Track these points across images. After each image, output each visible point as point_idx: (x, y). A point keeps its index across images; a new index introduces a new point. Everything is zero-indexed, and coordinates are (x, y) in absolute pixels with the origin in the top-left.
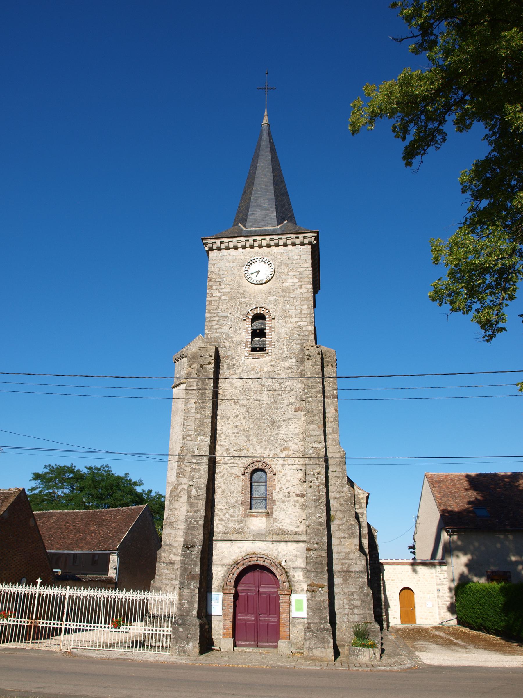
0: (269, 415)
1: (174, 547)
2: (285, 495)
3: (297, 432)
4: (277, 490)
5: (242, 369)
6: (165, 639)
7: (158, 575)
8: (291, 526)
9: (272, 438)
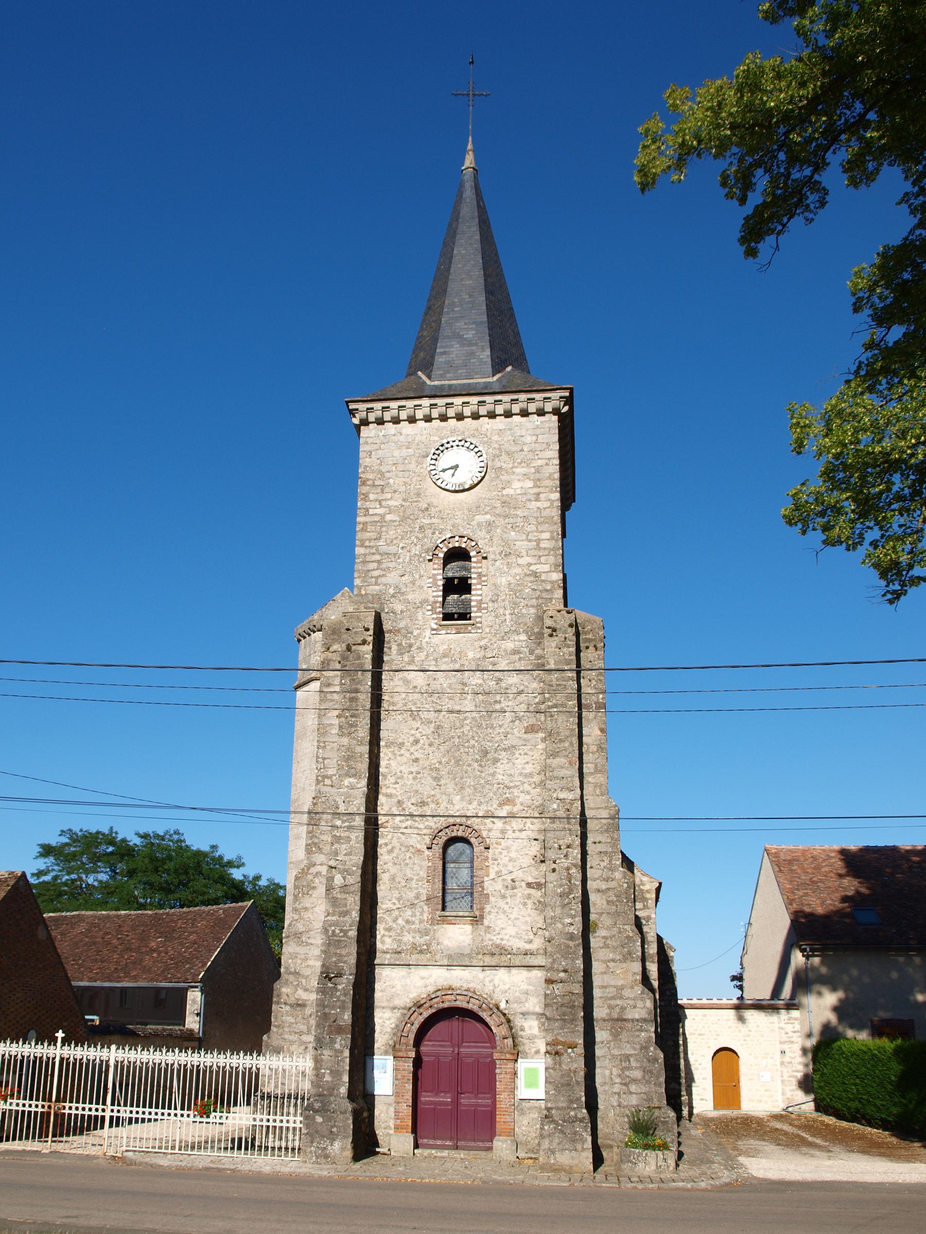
0: (476, 739)
1: (303, 976)
4: (492, 875)
6: (290, 1136)
7: (275, 1026)
8: (517, 940)
9: (482, 782)
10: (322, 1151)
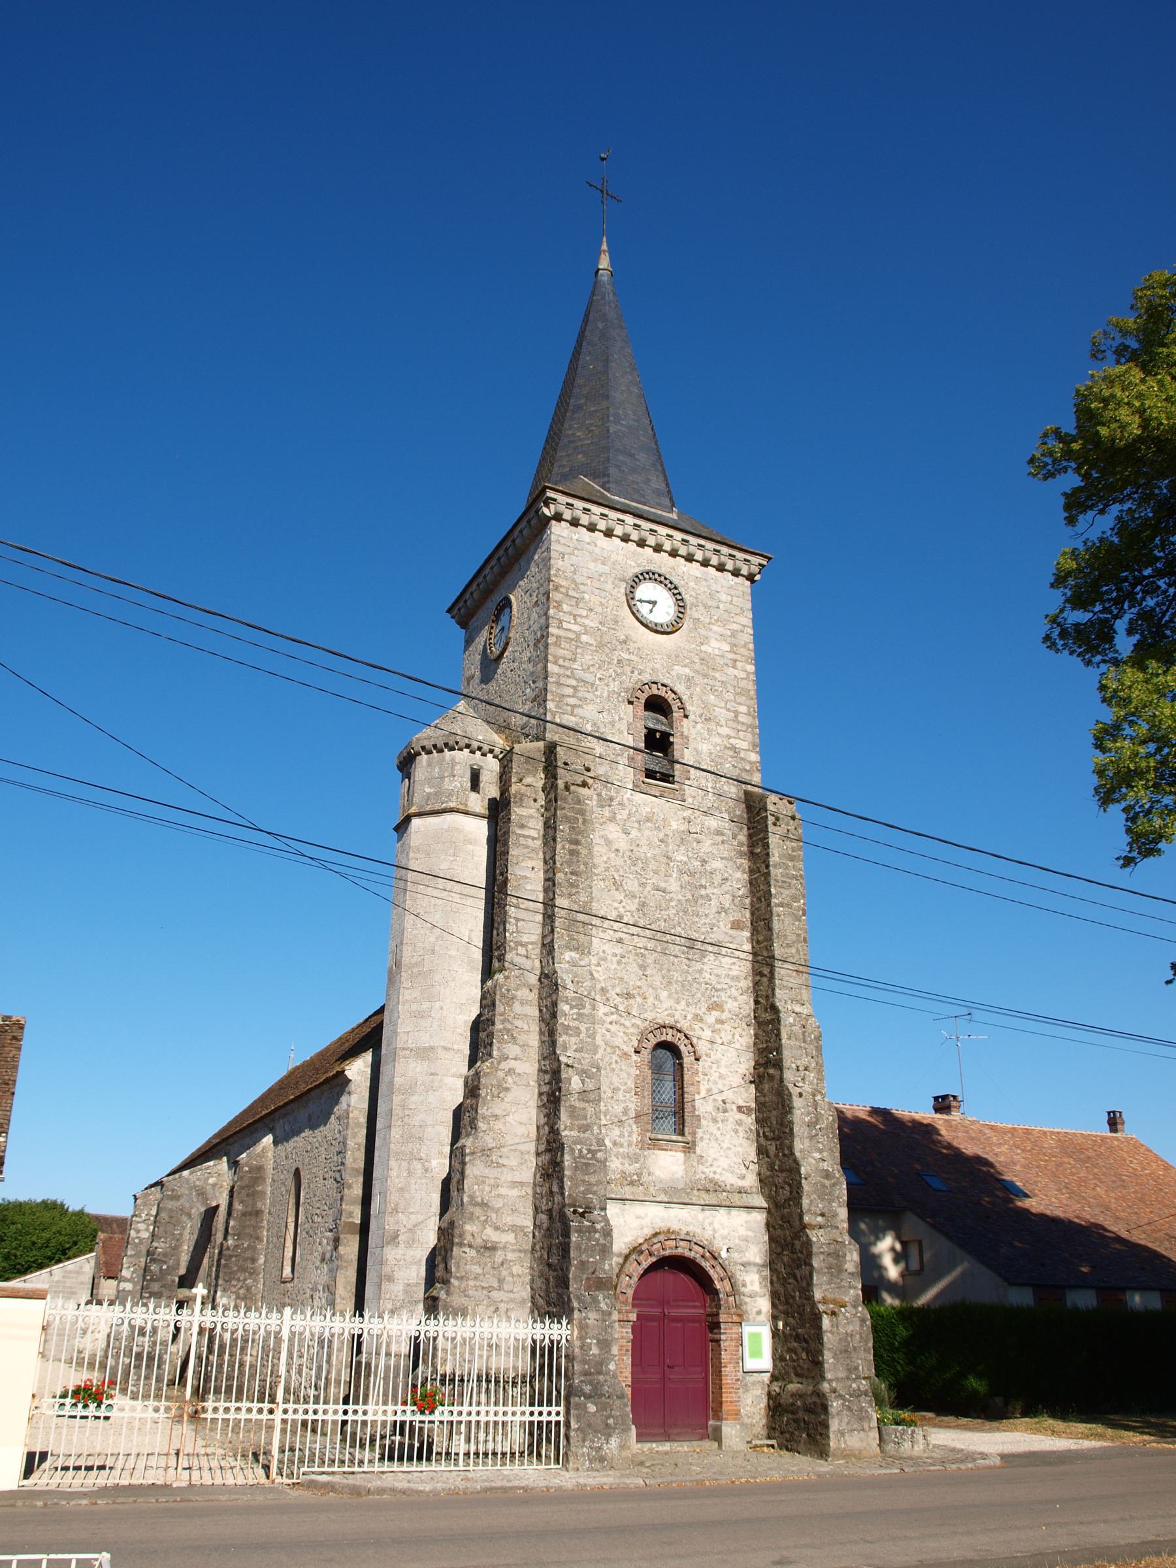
0: (683, 926)
1: (493, 1209)
2: (717, 1105)
3: (734, 973)
4: (703, 1094)
5: (627, 812)
6: (482, 1436)
7: (457, 1278)
8: (730, 1175)
9: (690, 978)
10: (597, 1452)
